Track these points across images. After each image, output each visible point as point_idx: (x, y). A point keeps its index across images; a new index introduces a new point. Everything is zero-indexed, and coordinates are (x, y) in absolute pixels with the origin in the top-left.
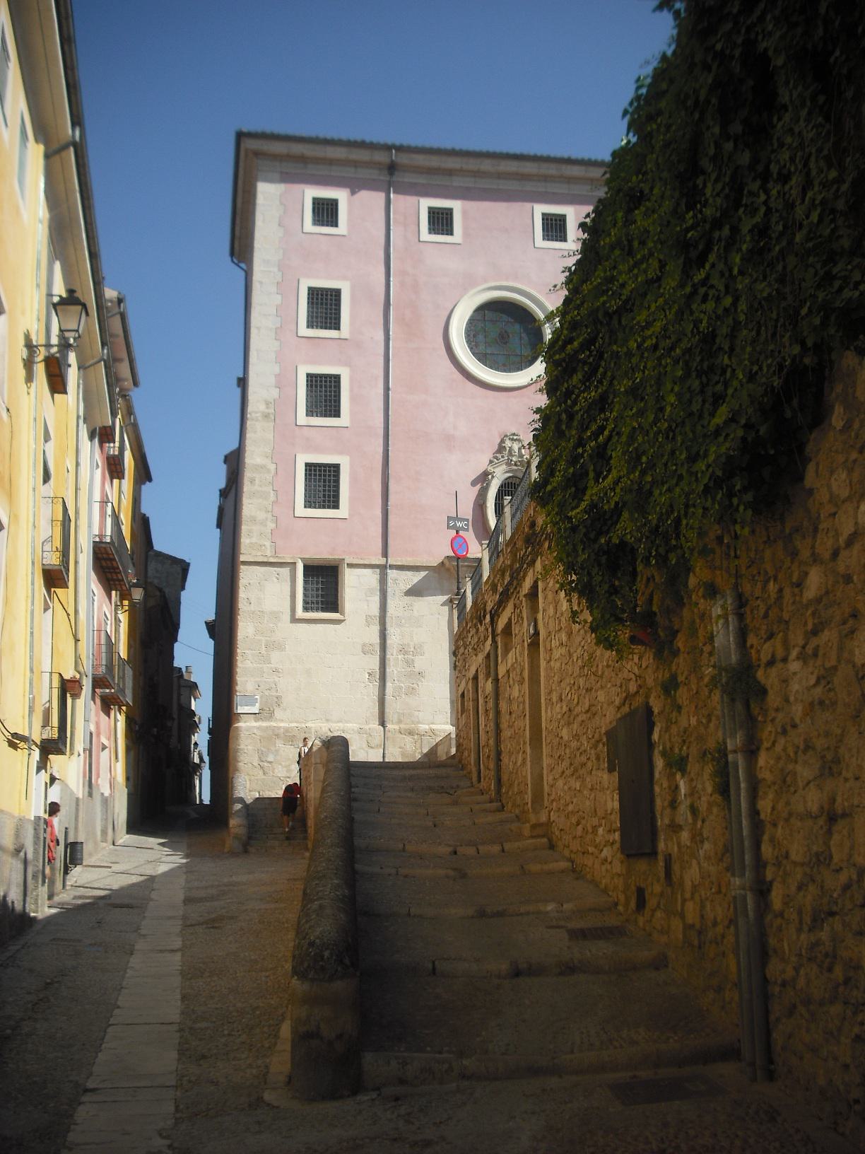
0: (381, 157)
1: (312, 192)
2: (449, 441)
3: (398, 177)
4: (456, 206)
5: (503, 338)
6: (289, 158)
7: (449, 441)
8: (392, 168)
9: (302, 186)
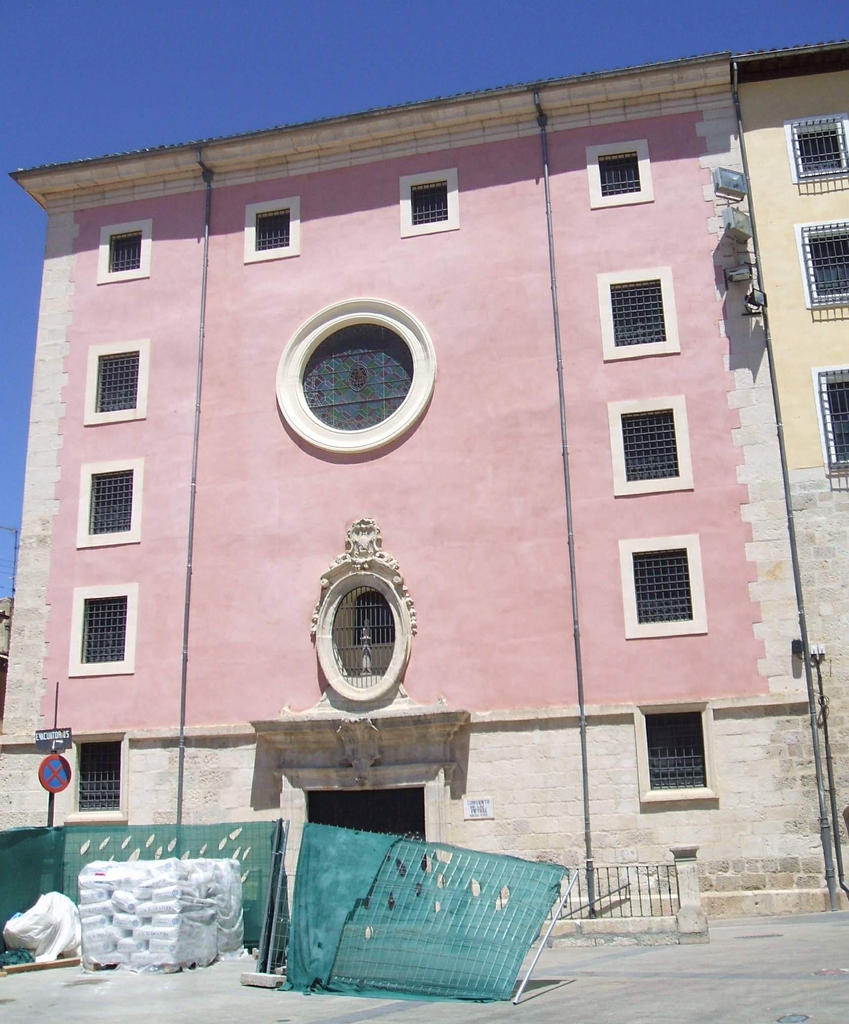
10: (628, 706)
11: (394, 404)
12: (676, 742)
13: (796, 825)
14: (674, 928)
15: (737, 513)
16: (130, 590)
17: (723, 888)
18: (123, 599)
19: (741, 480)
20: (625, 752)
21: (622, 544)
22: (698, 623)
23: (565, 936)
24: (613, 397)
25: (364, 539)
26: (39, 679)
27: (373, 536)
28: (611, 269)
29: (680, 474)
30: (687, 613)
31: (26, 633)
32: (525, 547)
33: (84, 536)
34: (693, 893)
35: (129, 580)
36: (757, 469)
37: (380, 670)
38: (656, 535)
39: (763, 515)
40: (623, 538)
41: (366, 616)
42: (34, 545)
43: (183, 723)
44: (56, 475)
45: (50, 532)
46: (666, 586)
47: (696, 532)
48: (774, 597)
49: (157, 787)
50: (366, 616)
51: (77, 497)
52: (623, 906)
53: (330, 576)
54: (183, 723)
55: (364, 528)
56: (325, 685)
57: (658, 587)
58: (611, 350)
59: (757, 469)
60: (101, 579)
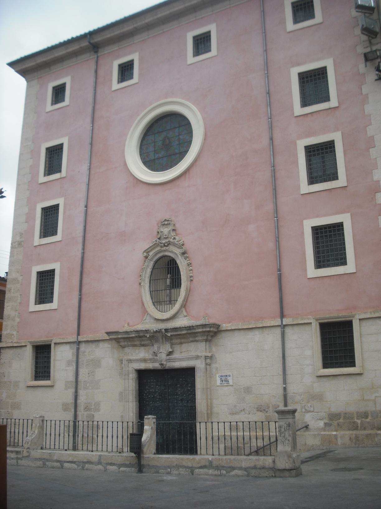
10: (308, 319)
11: (182, 154)
14: (271, 465)
15: (373, 199)
16: (56, 266)
17: (365, 429)
18: (53, 271)
19: (375, 178)
20: (307, 346)
21: (349, 215)
22: (350, 267)
23: (201, 467)
24: (300, 137)
25: (166, 230)
26: (17, 313)
27: (171, 228)
28: (299, 64)
29: (339, 178)
30: (343, 262)
31: (12, 291)
32: (251, 228)
33: (37, 241)
34: (287, 442)
35: (55, 261)
37: (171, 302)
38: (326, 215)
40: (306, 219)
41: (167, 273)
42: (17, 246)
43: (78, 334)
44: (368, 109)
45: (23, 239)
46: (331, 245)
47: (348, 212)
49: (67, 368)
50: (167, 273)
51: (34, 220)
52: (269, 443)
53: (147, 251)
54: (78, 334)
55: (165, 223)
56: (145, 311)
57: (327, 246)
58: (298, 110)
60: (44, 261)
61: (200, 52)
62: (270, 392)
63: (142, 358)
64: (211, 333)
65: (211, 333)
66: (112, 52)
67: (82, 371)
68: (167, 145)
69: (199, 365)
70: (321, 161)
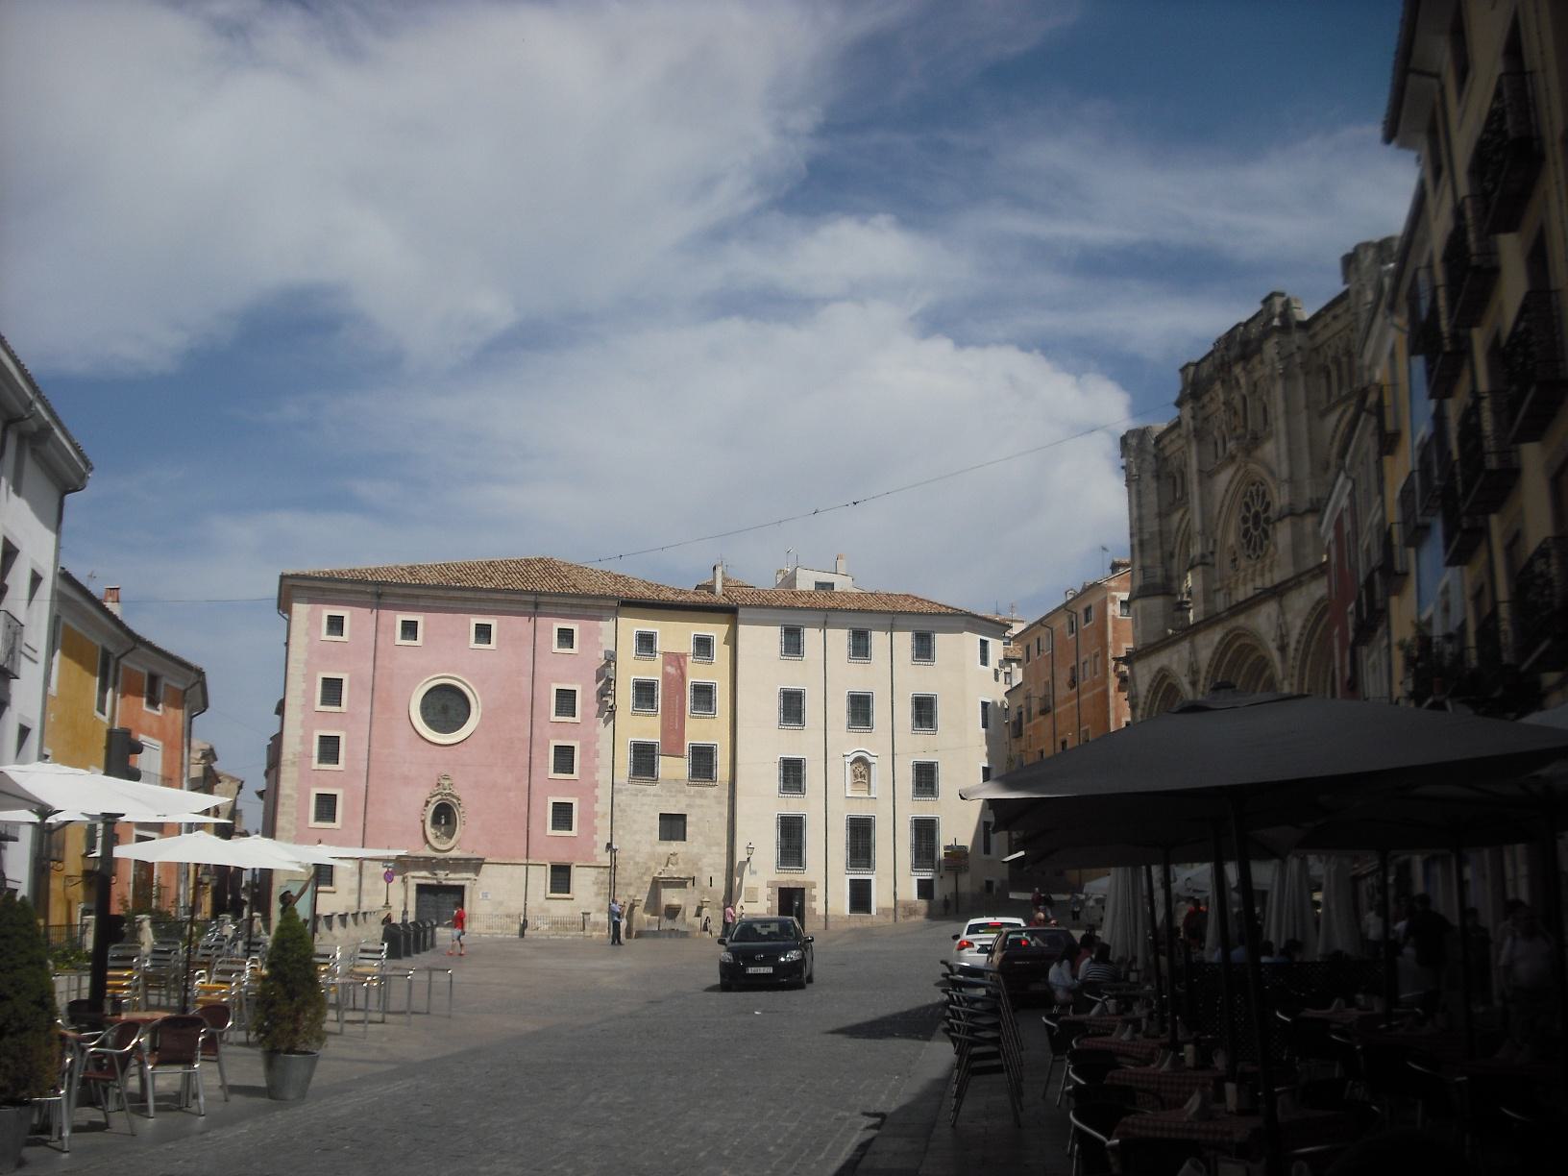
0: (532, 598)
1: (329, 611)
2: (406, 780)
3: (542, 609)
4: (492, 621)
5: (445, 710)
6: (309, 588)
7: (406, 780)
8: (379, 596)
9: (391, 612)
12: (561, 877)
13: (600, 910)
20: (541, 878)
22: (574, 832)
36: (603, 776)
39: (603, 793)
41: (444, 815)
48: (602, 824)
50: (444, 815)
56: (427, 842)
59: (603, 776)
61: (1062, 622)
62: (516, 906)
63: (422, 876)
64: (475, 865)
65: (475, 865)
66: (331, 590)
67: (365, 882)
68: (445, 710)
69: (467, 883)
70: (564, 758)
